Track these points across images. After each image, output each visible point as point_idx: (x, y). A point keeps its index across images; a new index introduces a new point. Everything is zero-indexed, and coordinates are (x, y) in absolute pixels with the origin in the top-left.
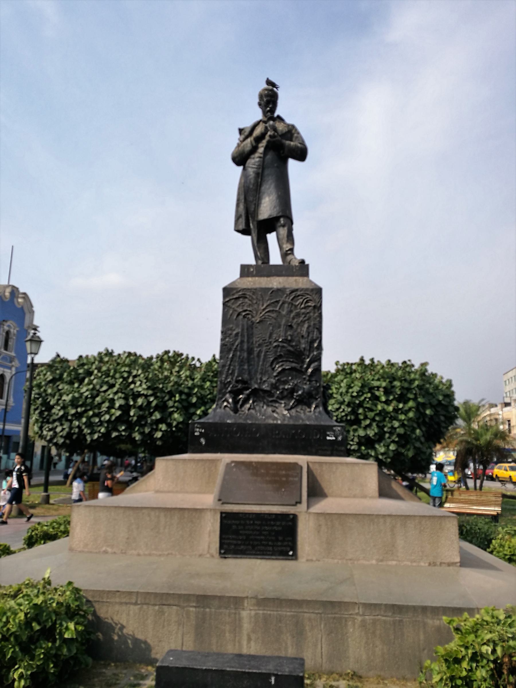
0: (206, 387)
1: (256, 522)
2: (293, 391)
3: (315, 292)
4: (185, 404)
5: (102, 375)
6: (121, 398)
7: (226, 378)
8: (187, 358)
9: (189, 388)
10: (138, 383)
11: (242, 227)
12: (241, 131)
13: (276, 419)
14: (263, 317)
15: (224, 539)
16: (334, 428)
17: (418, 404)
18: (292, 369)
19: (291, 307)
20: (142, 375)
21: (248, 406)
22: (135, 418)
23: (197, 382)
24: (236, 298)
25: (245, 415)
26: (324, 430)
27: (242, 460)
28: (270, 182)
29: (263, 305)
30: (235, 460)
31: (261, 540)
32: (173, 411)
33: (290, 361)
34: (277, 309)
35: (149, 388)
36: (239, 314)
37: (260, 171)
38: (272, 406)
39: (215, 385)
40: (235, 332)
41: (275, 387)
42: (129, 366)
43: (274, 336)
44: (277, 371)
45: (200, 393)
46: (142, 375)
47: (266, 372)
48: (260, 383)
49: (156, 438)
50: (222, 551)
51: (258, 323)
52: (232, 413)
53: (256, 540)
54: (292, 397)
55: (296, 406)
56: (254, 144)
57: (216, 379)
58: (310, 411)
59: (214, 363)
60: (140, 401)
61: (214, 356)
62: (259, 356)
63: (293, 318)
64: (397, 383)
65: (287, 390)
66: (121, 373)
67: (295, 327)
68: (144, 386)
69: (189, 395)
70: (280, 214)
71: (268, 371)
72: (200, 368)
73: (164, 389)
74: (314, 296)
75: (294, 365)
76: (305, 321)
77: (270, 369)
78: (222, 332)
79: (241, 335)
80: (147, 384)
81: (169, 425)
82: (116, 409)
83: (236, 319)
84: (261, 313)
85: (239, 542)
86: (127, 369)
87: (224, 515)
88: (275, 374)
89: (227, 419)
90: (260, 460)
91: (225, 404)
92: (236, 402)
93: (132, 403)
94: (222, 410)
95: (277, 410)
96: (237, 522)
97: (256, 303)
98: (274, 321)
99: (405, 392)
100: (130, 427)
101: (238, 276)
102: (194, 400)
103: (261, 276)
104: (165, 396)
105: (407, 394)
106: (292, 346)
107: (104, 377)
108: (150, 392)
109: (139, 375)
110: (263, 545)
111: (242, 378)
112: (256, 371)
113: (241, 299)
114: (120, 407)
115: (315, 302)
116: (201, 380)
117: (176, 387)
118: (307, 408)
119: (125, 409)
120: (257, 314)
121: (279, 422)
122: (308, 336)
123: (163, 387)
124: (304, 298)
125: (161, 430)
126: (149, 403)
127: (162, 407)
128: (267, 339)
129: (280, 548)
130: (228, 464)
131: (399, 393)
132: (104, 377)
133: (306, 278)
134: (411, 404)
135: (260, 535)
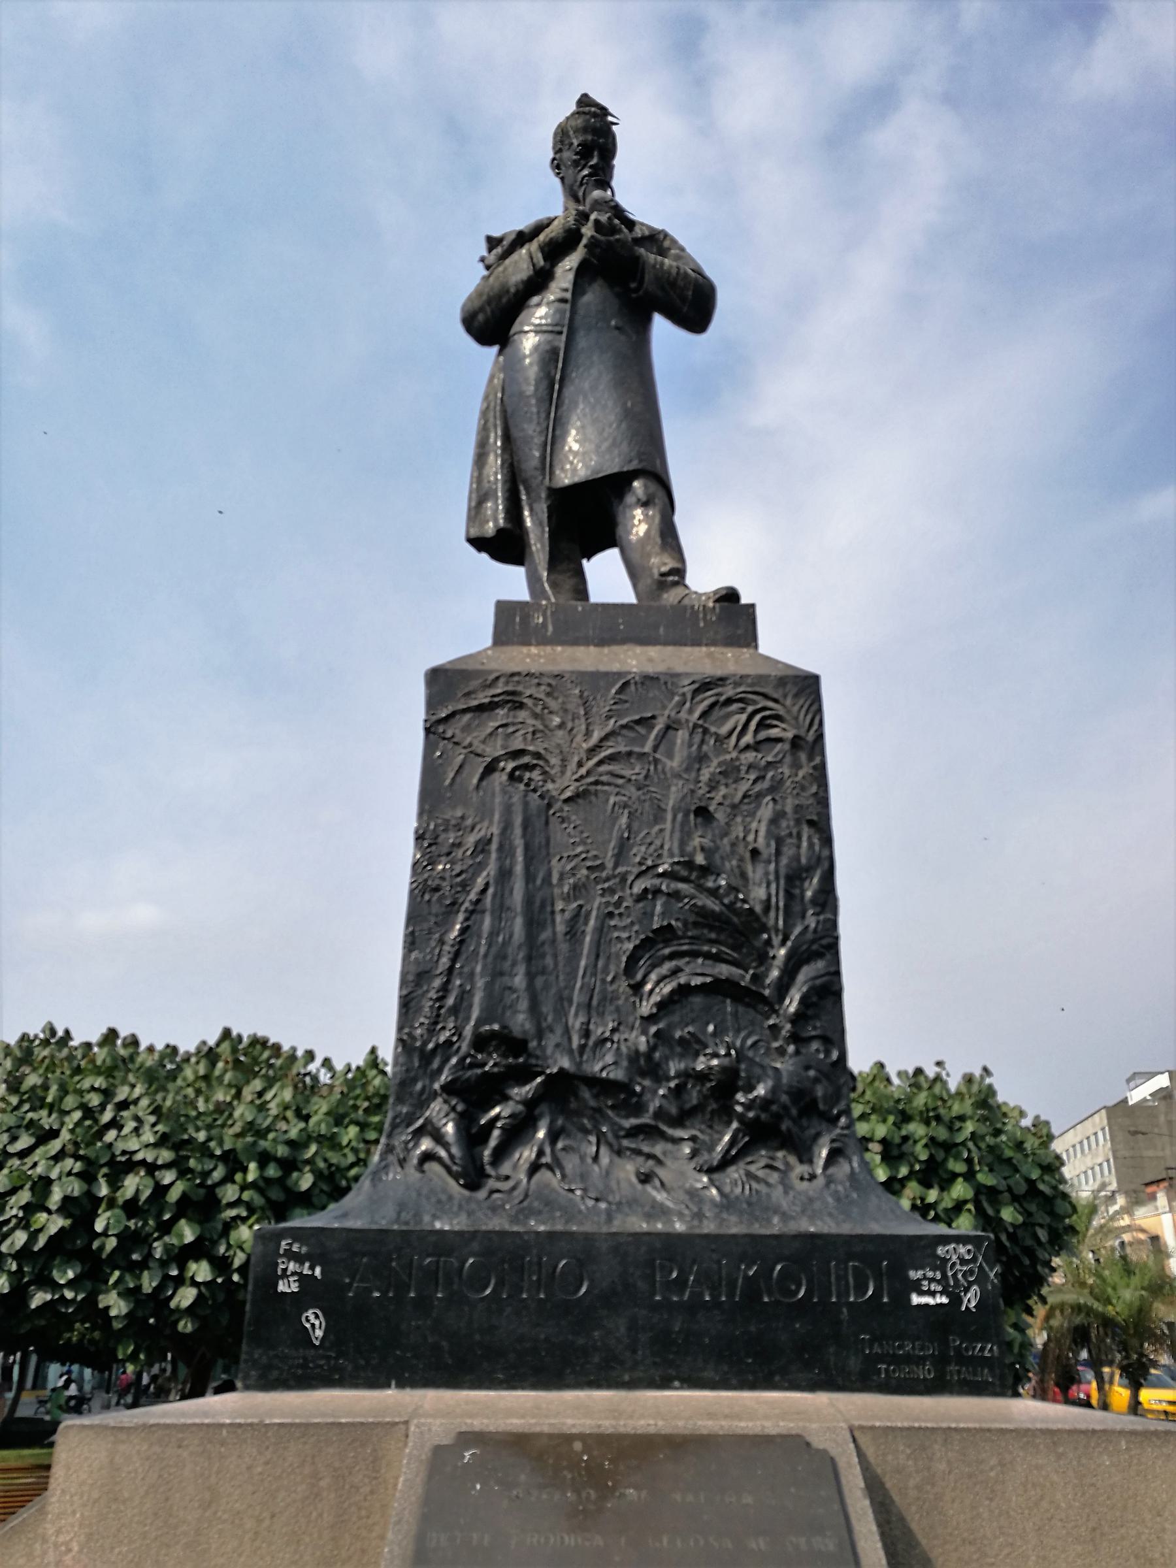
0: (345, 1142)
2: (728, 1083)
3: (792, 689)
4: (276, 1194)
5: (21, 1102)
6: (69, 1174)
7: (432, 1031)
8: (292, 1057)
9: (291, 1143)
10: (130, 1125)
11: (495, 519)
12: (492, 243)
13: (657, 1211)
14: (591, 779)
16: (940, 1251)
17: (980, 1189)
18: (719, 988)
19: (703, 742)
20: (144, 1102)
21: (527, 1154)
22: (112, 1243)
23: (319, 1123)
24: (481, 708)
25: (518, 1194)
26: (894, 1258)
27: (516, 1424)
28: (594, 371)
29: (588, 734)
30: (477, 1424)
32: (238, 1217)
33: (708, 956)
34: (647, 748)
35: (162, 1141)
36: (490, 769)
37: (561, 342)
38: (638, 1152)
39: (372, 1136)
40: (471, 840)
41: (647, 1066)
42: (108, 1072)
43: (638, 852)
44: (655, 998)
45: (326, 1160)
46: (144, 1102)
47: (607, 999)
48: (582, 1048)
49: (177, 1309)
51: (566, 801)
52: (454, 1187)
54: (726, 1113)
56: (540, 261)
57: (376, 1119)
58: (813, 1177)
59: (372, 1073)
60: (131, 1184)
61: (373, 1051)
62: (573, 932)
63: (713, 786)
64: (916, 1129)
65: (702, 1077)
66: (80, 1093)
67: (720, 816)
68: (149, 1137)
69: (290, 1165)
70: (634, 465)
71: (615, 997)
72: (331, 1087)
73: (212, 1144)
74: (788, 702)
75: (724, 970)
76: (760, 795)
77: (623, 985)
78: (419, 838)
79: (501, 848)
80: (159, 1127)
81: (221, 1265)
82: (49, 1212)
83: (478, 787)
84: (580, 765)
86: (99, 1082)
88: (646, 1008)
89: (435, 1217)
90: (607, 1425)
91: (426, 1144)
92: (473, 1136)
93: (104, 1191)
94: (412, 1174)
95: (661, 1172)
97: (561, 726)
98: (632, 791)
99: (940, 1155)
100: (94, 1272)
101: (489, 642)
102: (306, 1181)
103: (575, 642)
104: (215, 1168)
105: (945, 1160)
106: (714, 893)
107: (26, 1107)
108: (166, 1155)
109: (136, 1102)
111: (504, 1027)
112: (563, 1001)
113: (501, 712)
114: (68, 1204)
115: (797, 727)
116: (331, 1120)
117: (249, 1139)
118: (792, 1159)
119: (81, 1210)
120: (564, 767)
121: (679, 1227)
122: (778, 853)
123: (209, 1139)
124: (750, 709)
125: (194, 1283)
126: (161, 1191)
127: (201, 1205)
128: (610, 864)
130: (438, 1450)
131: (924, 1157)
132: (26, 1107)
133: (746, 652)
134: (960, 1190)
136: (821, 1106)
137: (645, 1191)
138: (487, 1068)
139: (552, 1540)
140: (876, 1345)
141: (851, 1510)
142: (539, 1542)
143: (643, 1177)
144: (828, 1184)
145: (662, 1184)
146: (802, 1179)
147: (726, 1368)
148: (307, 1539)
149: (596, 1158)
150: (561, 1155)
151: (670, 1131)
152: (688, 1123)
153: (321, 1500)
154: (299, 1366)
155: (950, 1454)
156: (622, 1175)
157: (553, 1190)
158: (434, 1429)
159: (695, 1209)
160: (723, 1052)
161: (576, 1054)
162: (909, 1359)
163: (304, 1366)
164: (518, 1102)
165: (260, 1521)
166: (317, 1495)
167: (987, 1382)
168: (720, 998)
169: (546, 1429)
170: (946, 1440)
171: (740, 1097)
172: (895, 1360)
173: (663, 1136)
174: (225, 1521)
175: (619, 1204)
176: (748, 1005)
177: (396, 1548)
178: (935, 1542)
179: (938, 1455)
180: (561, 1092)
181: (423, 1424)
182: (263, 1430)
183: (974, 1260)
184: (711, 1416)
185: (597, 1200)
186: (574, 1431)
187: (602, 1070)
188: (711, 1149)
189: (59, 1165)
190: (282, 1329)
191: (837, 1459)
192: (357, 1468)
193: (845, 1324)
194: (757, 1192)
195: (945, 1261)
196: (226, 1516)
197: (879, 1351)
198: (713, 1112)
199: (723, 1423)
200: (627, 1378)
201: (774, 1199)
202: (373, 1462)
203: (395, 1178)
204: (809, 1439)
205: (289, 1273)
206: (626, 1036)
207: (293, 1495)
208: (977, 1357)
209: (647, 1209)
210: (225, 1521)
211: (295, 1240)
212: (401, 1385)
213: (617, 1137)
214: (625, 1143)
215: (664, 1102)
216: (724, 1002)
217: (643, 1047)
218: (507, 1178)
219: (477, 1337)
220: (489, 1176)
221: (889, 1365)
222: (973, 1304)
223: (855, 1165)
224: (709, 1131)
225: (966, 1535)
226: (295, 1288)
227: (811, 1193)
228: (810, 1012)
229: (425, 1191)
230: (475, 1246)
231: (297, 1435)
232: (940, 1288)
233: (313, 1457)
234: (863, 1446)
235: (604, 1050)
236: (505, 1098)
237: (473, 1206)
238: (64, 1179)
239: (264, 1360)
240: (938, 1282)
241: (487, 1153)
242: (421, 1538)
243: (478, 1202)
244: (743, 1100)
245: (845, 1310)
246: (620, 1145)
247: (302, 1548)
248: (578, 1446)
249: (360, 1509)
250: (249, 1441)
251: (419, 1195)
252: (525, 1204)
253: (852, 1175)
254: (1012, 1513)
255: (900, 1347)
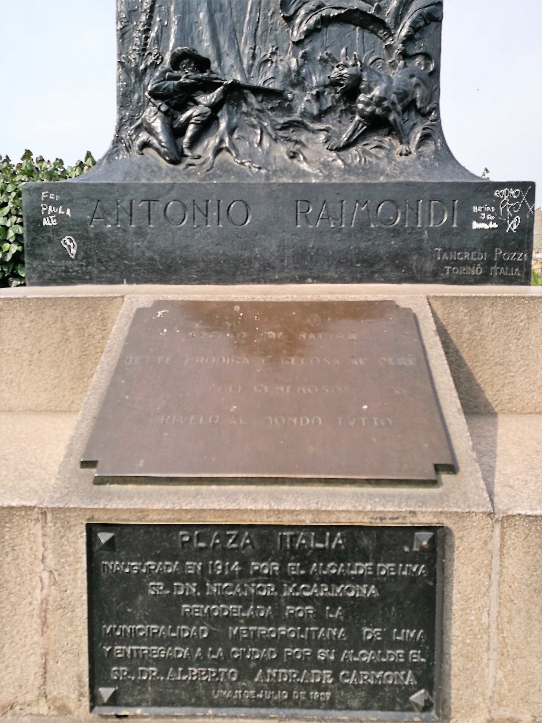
1: (255, 566)
6: (15, 224)
15: (113, 640)
25: (207, 166)
31: (282, 642)
38: (289, 140)
44: (304, 27)
50: (106, 692)
52: (164, 163)
53: (264, 642)
54: (351, 111)
55: (363, 136)
82: (10, 243)
85: (183, 652)
87: (104, 537)
88: (296, 35)
90: (259, 298)
92: (176, 132)
96: (172, 568)
110: (292, 663)
118: (395, 142)
129: (367, 677)
130: (140, 311)
135: (276, 620)
136: (418, 104)
137: (293, 163)
138: (181, 80)
139: (214, 360)
140: (445, 255)
141: (425, 342)
142: (204, 361)
143: (292, 154)
144: (419, 157)
145: (305, 158)
146: (401, 154)
147: (343, 270)
148: (64, 365)
149: (260, 143)
150: (236, 142)
151: (312, 126)
152: (324, 119)
153: (70, 343)
154: (62, 271)
155: (494, 312)
156: (277, 154)
157: (230, 164)
158: (140, 300)
159: (327, 173)
160: (350, 63)
161: (246, 73)
162: (466, 263)
163: (66, 271)
164: (206, 106)
165: (32, 355)
166: (67, 340)
167: (516, 277)
168: (353, 27)
169: (217, 300)
170: (493, 304)
171: (361, 97)
172: (457, 264)
173: (306, 127)
174: (9, 355)
175: (275, 172)
176: (372, 32)
177: (106, 366)
178: (477, 364)
179: (486, 313)
180: (235, 93)
181: (133, 298)
182: (27, 302)
183: (520, 198)
184: (330, 293)
185: (260, 168)
186: (236, 300)
187: (264, 82)
188: (339, 136)
189: (10, 220)
190: (49, 248)
191: (417, 314)
192: (92, 324)
193: (425, 241)
194: (369, 162)
195: (499, 199)
196: (9, 352)
197: (447, 258)
198: (341, 111)
199: (338, 296)
200: (277, 277)
201: (381, 167)
202: (102, 320)
203: (123, 158)
204: (397, 303)
205: (49, 213)
206: (282, 58)
207: (52, 340)
208: (512, 261)
209: (293, 173)
210: (9, 355)
211: (50, 191)
212: (130, 282)
213: (275, 129)
214: (280, 133)
215: (308, 104)
216: (354, 29)
217: (294, 65)
218: (199, 157)
219: (178, 252)
220: (186, 156)
221: (453, 267)
222: (515, 227)
223: (439, 144)
224: (338, 124)
225: (498, 360)
226: (54, 222)
227: (407, 163)
228: (417, 36)
229: (143, 166)
230: (174, 194)
231: (50, 304)
232: (493, 218)
233: (62, 317)
234: (435, 309)
235: (266, 68)
236: (197, 103)
237: (175, 173)
238: (13, 226)
239: (40, 268)
240: (492, 214)
241: (186, 140)
242: (122, 360)
243: (178, 171)
244: (362, 99)
245: (426, 232)
246: (276, 134)
247: (61, 369)
248: (237, 308)
249: (96, 348)
250: (18, 308)
251: (139, 167)
252: (211, 172)
253: (436, 151)
254: (531, 347)
255: (461, 256)
